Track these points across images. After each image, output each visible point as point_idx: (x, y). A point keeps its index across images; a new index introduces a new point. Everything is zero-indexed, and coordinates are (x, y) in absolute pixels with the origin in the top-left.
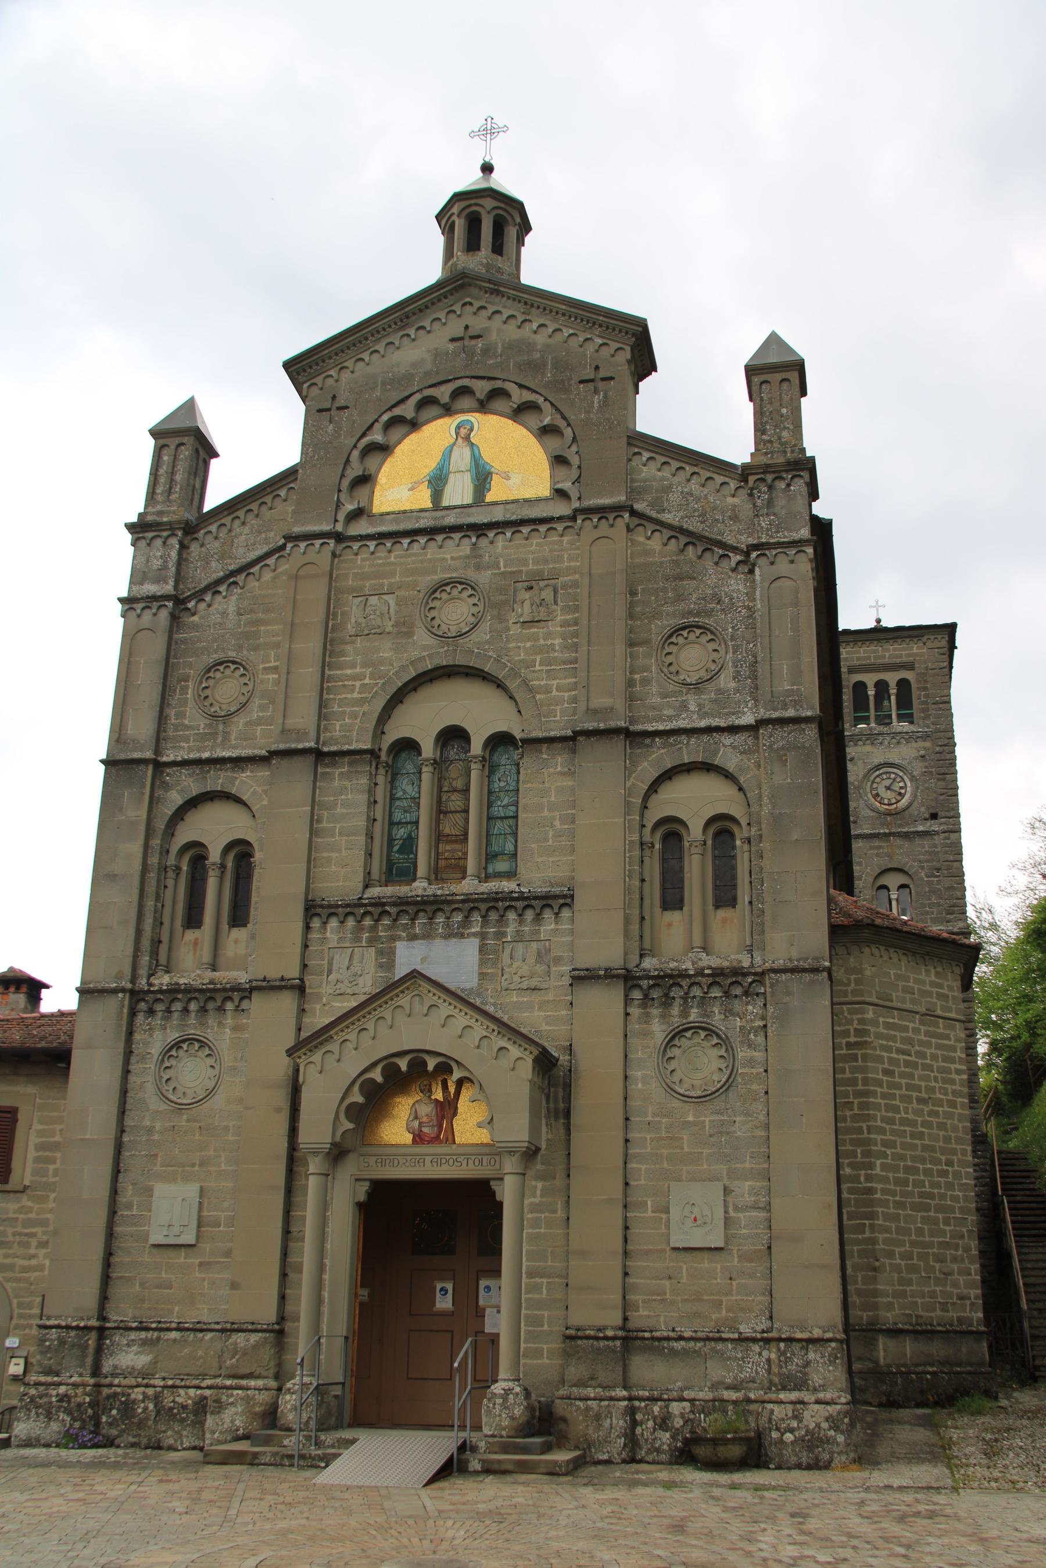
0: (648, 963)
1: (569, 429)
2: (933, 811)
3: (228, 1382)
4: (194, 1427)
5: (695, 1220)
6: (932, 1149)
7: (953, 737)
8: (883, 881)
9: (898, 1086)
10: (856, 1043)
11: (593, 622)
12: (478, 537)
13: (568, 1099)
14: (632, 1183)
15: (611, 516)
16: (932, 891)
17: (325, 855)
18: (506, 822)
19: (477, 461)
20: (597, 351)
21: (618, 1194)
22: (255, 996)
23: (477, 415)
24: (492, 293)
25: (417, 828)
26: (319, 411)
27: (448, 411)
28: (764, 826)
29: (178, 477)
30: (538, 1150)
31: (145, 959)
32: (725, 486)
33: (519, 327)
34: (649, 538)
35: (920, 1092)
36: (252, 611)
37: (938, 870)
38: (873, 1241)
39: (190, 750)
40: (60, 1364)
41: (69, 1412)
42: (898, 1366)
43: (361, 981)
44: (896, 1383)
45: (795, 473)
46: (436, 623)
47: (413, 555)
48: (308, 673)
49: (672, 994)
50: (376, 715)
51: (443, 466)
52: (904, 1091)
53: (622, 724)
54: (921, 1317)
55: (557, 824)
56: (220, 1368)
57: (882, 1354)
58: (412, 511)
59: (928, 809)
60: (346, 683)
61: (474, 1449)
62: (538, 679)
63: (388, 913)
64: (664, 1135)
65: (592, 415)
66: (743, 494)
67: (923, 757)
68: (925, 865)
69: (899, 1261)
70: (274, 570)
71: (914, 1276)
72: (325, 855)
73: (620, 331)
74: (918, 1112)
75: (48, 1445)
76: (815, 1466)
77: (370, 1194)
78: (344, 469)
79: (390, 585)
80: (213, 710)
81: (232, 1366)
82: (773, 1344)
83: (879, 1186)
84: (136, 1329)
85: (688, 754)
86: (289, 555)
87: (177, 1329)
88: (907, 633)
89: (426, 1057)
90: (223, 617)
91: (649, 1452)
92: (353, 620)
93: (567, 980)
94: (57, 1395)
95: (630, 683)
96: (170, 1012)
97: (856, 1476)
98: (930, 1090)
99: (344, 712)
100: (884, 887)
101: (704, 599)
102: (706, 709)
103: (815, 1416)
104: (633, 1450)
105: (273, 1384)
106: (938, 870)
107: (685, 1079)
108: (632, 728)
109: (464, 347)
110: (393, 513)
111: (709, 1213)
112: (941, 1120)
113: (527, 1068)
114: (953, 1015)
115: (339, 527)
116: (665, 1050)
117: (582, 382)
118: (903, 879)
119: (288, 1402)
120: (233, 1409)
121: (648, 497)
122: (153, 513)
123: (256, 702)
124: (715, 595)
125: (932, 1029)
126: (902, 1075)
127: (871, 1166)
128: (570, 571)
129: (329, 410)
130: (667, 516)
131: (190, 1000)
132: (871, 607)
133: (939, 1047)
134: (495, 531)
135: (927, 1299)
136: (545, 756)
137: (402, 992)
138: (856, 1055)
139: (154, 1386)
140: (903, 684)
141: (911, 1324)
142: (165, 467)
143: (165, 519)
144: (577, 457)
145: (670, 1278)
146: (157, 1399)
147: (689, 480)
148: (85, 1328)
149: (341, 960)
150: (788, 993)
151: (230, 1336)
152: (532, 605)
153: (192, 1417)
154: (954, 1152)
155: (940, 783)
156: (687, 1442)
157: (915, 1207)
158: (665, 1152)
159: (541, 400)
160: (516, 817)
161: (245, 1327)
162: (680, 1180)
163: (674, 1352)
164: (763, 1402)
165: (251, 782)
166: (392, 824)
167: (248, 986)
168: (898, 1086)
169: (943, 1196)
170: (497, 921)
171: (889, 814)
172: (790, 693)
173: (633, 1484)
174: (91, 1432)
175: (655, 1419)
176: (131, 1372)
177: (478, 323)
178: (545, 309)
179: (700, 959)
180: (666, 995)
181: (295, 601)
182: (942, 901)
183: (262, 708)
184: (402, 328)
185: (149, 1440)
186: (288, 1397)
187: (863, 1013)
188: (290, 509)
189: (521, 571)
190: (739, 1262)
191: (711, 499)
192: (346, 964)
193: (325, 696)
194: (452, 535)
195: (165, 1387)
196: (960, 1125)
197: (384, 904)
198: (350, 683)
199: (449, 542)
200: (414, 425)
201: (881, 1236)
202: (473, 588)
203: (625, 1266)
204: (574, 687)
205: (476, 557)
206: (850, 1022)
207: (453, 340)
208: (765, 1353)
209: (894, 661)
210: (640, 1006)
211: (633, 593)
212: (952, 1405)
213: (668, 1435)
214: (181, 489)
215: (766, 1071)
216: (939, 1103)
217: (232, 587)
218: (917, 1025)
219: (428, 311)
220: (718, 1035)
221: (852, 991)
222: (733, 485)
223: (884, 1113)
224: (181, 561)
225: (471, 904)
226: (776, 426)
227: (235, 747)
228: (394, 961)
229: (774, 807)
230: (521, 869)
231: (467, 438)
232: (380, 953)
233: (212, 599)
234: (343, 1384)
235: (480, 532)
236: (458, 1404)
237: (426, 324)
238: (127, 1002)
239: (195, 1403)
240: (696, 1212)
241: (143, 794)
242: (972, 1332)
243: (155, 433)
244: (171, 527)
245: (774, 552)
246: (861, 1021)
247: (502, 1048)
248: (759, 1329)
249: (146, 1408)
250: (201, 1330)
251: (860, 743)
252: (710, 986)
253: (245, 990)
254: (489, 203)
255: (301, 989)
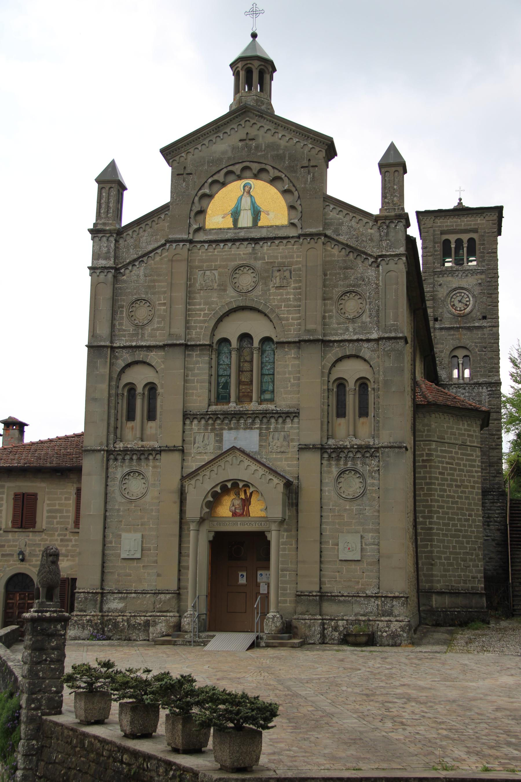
0: (331, 442)
1: (297, 192)
2: (484, 315)
3: (158, 614)
4: (144, 632)
5: (349, 549)
6: (462, 509)
7: (497, 273)
8: (454, 354)
9: (447, 480)
10: (427, 460)
11: (308, 289)
12: (255, 244)
13: (297, 498)
14: (323, 533)
15: (316, 238)
16: (481, 359)
17: (191, 391)
18: (269, 376)
19: (253, 204)
20: (310, 151)
21: (318, 538)
22: (163, 454)
23: (253, 180)
24: (259, 117)
25: (230, 378)
26: (178, 175)
27: (239, 178)
28: (380, 385)
29: (111, 205)
30: (285, 519)
31: (112, 436)
32: (367, 224)
33: (273, 136)
34: (333, 248)
35: (457, 482)
36: (151, 275)
37: (485, 348)
38: (431, 552)
39: (126, 341)
40: (86, 607)
41: (92, 626)
42: (442, 608)
43: (208, 447)
44: (440, 616)
45: (399, 220)
46: (237, 285)
47: (225, 251)
48: (180, 308)
49: (340, 456)
50: (211, 328)
51: (238, 206)
52: (449, 482)
53: (320, 337)
54: (454, 586)
55: (292, 380)
56: (154, 608)
57: (434, 603)
58: (224, 229)
59: (481, 313)
60: (197, 312)
61: (262, 638)
62: (283, 314)
63: (219, 418)
64: (337, 514)
65: (307, 186)
66: (376, 228)
67: (480, 284)
68: (478, 345)
69: (444, 561)
70: (161, 256)
71: (451, 568)
72: (191, 391)
73: (320, 142)
74: (455, 492)
75: (84, 639)
76: (395, 645)
77: (214, 537)
78: (192, 207)
79: (215, 265)
80: (136, 322)
81: (159, 607)
82: (379, 598)
83: (435, 527)
84: (117, 593)
85: (349, 350)
86: (168, 249)
87: (135, 593)
88: (475, 211)
89: (239, 482)
90: (138, 278)
91: (330, 640)
92: (199, 282)
93: (296, 449)
94: (86, 620)
95: (324, 317)
96: (124, 460)
97: (410, 648)
98: (462, 481)
99: (196, 326)
100: (455, 356)
101: (356, 279)
102: (356, 331)
103: (395, 626)
104: (323, 639)
105: (177, 614)
106: (485, 348)
107: (346, 491)
108: (324, 339)
109: (247, 144)
110: (215, 229)
111: (355, 546)
112: (467, 495)
113: (281, 488)
114: (475, 444)
115: (191, 237)
116: (337, 479)
117: (302, 167)
118: (466, 353)
119: (185, 621)
120: (161, 625)
121: (333, 228)
122: (101, 224)
123: (156, 320)
124: (361, 277)
125: (464, 452)
126: (449, 474)
127: (431, 517)
128: (297, 263)
129: (182, 174)
130: (341, 237)
131: (133, 454)
132: (456, 191)
133: (467, 460)
134: (263, 242)
135: (457, 578)
136: (286, 350)
137: (229, 455)
138: (427, 465)
139: (126, 616)
140: (471, 241)
141: (448, 590)
142: (104, 199)
143: (108, 228)
144: (300, 207)
145: (339, 572)
146: (128, 621)
147: (351, 220)
148: (96, 593)
149: (199, 438)
150: (389, 457)
151: (158, 596)
152: (280, 279)
153: (143, 628)
154: (473, 510)
155: (488, 299)
156: (345, 636)
157: (453, 536)
158: (337, 521)
159: (283, 176)
160: (273, 374)
161: (164, 592)
162: (343, 532)
163: (340, 601)
164: (375, 621)
165: (155, 357)
166: (218, 376)
167: (159, 449)
168: (447, 480)
169: (466, 531)
170: (267, 423)
171: (460, 316)
172: (393, 325)
173: (324, 650)
174: (101, 634)
175: (332, 627)
176: (116, 610)
177: (253, 132)
178: (285, 128)
179: (352, 441)
180: (338, 456)
181: (172, 272)
182: (487, 365)
183: (159, 322)
184: (216, 133)
185: (126, 637)
186: (185, 619)
187: (430, 446)
188: (167, 225)
189: (275, 262)
190: (367, 565)
191: (361, 230)
192: (202, 440)
193: (188, 318)
194: (243, 243)
195: (131, 616)
196: (477, 497)
197: (217, 414)
198: (199, 312)
199: (242, 246)
200: (224, 184)
201: (435, 550)
202: (253, 269)
203: (320, 567)
204: (299, 318)
205: (254, 254)
206: (424, 450)
207: (241, 140)
208: (376, 602)
209: (466, 227)
210: (327, 460)
211: (325, 275)
212: (466, 626)
213: (337, 633)
214: (113, 212)
215: (379, 488)
216: (467, 487)
217: (141, 263)
218: (457, 450)
219: (229, 124)
220: (359, 474)
221: (426, 435)
222: (371, 224)
223: (439, 493)
224: (116, 248)
225: (255, 415)
226: (391, 195)
227: (147, 340)
228: (222, 439)
229: (384, 377)
230: (276, 399)
231: (249, 192)
232: (216, 435)
233: (132, 268)
234: (206, 614)
235: (256, 242)
236: (256, 621)
237: (228, 130)
238: (105, 455)
239: (144, 623)
240: (350, 546)
241: (106, 362)
242: (478, 593)
243: (98, 180)
244: (111, 232)
245: (388, 259)
246: (429, 450)
247: (270, 479)
248: (374, 592)
249: (123, 625)
250: (145, 593)
251: (445, 275)
252: (356, 453)
253: (158, 451)
254: (256, 63)
255: (182, 451)
